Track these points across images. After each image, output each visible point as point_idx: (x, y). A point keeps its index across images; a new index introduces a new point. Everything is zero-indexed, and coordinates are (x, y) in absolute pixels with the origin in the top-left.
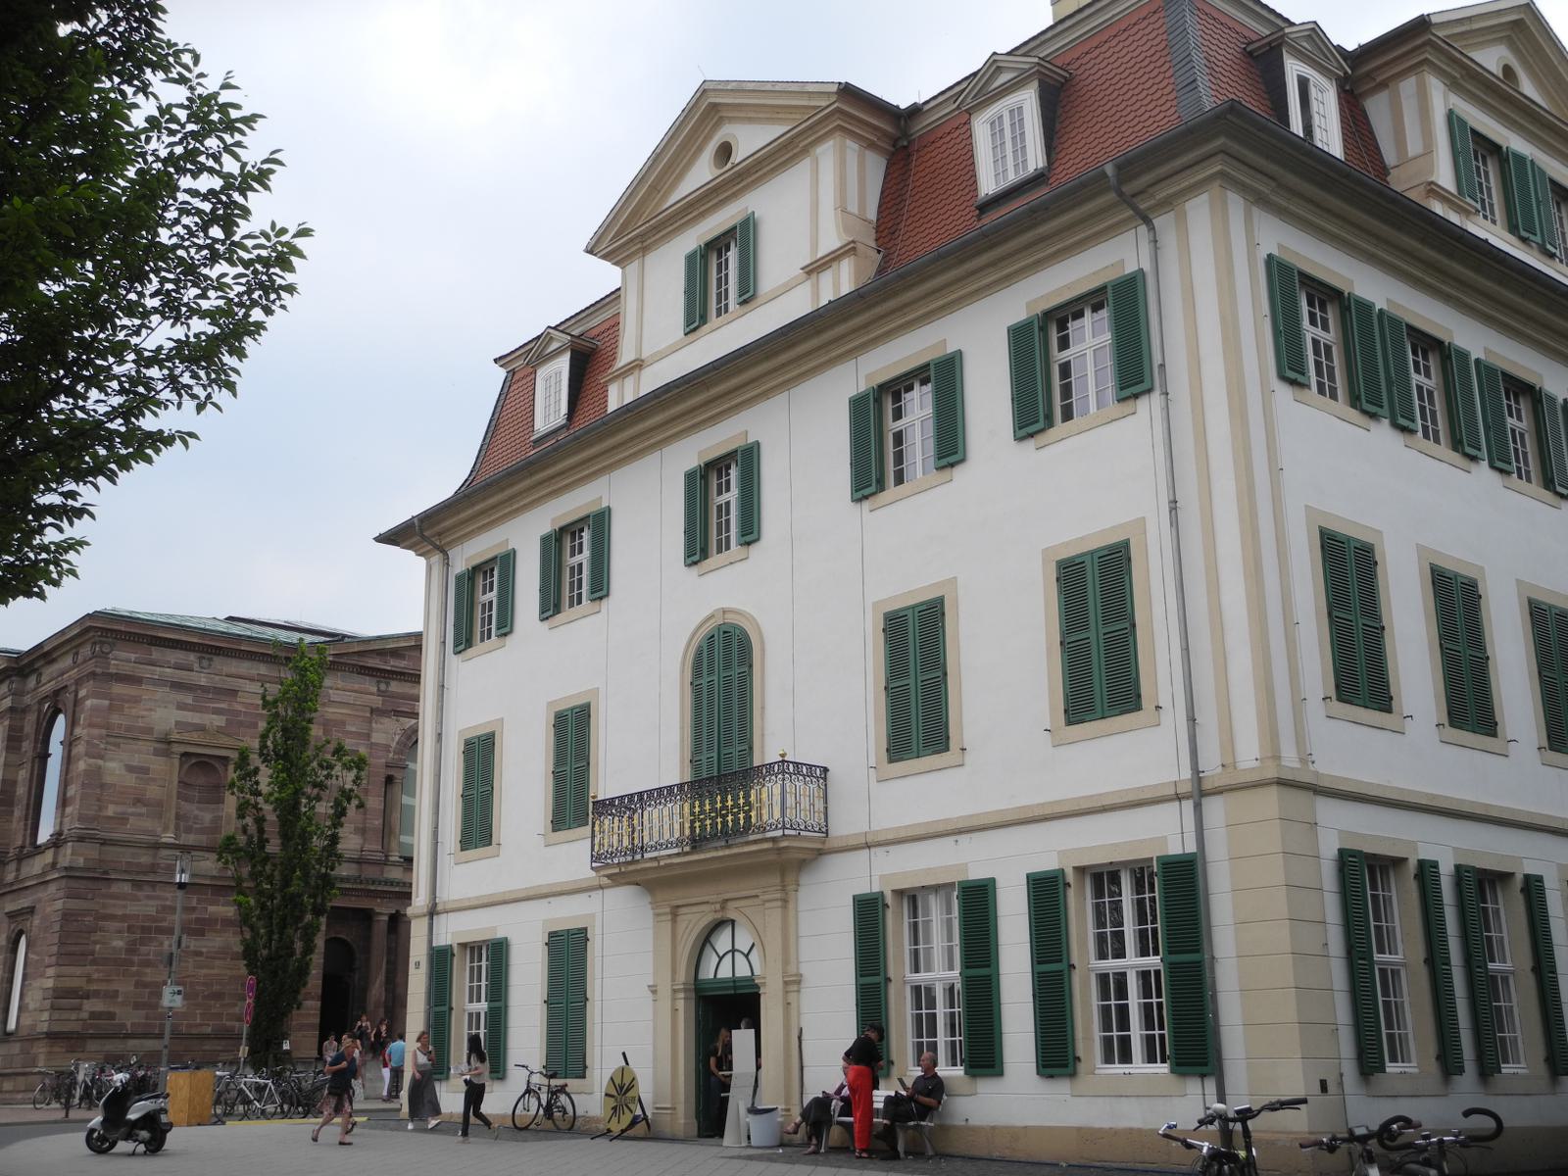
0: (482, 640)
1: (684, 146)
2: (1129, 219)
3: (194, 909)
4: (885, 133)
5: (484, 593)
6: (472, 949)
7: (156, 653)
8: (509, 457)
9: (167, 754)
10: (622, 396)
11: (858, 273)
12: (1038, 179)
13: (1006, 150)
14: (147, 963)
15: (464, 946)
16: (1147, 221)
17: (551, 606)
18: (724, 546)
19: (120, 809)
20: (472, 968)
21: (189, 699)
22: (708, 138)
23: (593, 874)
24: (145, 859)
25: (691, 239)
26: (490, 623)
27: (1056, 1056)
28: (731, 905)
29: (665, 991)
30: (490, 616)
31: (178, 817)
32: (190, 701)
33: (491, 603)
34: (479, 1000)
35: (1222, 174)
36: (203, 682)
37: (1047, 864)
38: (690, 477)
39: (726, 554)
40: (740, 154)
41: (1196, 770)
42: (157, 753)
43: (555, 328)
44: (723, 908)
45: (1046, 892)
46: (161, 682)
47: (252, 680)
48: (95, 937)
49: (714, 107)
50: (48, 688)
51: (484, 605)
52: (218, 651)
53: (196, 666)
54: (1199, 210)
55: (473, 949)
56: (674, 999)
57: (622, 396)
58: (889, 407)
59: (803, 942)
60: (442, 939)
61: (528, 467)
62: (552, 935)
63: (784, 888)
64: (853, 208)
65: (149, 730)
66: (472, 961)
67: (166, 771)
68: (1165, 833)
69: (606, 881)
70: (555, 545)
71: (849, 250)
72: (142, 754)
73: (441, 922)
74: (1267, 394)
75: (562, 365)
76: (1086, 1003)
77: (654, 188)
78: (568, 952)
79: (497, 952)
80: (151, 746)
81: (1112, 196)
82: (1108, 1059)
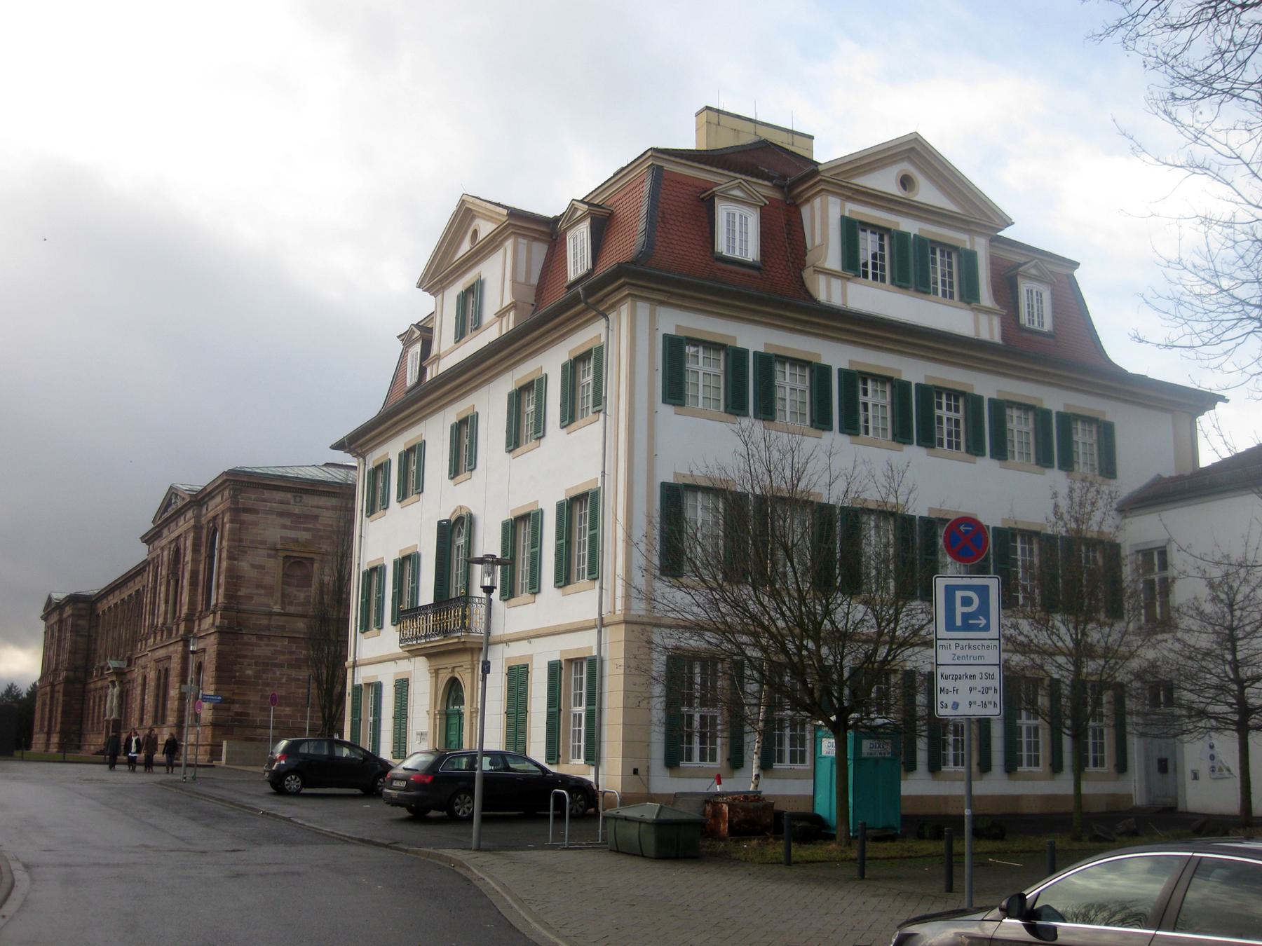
2: (595, 316)
3: (293, 653)
4: (543, 232)
7: (267, 494)
8: (399, 396)
9: (275, 557)
13: (578, 256)
14: (267, 685)
15: (570, 661)
17: (569, 416)
19: (249, 591)
21: (288, 522)
22: (466, 232)
24: (264, 622)
27: (1011, 766)
31: (283, 595)
32: (288, 523)
35: (629, 295)
36: (297, 511)
38: (510, 396)
40: (482, 236)
41: (600, 614)
42: (269, 556)
43: (582, 201)
44: (453, 671)
45: (555, 670)
46: (271, 512)
47: (327, 509)
48: (237, 667)
49: (468, 210)
50: (211, 514)
52: (306, 492)
53: (292, 501)
54: (625, 309)
60: (359, 681)
62: (510, 668)
64: (522, 278)
65: (264, 543)
67: (274, 566)
68: (585, 643)
71: (513, 306)
72: (260, 557)
74: (652, 412)
77: (446, 252)
78: (402, 687)
79: (377, 687)
80: (265, 552)
81: (582, 306)
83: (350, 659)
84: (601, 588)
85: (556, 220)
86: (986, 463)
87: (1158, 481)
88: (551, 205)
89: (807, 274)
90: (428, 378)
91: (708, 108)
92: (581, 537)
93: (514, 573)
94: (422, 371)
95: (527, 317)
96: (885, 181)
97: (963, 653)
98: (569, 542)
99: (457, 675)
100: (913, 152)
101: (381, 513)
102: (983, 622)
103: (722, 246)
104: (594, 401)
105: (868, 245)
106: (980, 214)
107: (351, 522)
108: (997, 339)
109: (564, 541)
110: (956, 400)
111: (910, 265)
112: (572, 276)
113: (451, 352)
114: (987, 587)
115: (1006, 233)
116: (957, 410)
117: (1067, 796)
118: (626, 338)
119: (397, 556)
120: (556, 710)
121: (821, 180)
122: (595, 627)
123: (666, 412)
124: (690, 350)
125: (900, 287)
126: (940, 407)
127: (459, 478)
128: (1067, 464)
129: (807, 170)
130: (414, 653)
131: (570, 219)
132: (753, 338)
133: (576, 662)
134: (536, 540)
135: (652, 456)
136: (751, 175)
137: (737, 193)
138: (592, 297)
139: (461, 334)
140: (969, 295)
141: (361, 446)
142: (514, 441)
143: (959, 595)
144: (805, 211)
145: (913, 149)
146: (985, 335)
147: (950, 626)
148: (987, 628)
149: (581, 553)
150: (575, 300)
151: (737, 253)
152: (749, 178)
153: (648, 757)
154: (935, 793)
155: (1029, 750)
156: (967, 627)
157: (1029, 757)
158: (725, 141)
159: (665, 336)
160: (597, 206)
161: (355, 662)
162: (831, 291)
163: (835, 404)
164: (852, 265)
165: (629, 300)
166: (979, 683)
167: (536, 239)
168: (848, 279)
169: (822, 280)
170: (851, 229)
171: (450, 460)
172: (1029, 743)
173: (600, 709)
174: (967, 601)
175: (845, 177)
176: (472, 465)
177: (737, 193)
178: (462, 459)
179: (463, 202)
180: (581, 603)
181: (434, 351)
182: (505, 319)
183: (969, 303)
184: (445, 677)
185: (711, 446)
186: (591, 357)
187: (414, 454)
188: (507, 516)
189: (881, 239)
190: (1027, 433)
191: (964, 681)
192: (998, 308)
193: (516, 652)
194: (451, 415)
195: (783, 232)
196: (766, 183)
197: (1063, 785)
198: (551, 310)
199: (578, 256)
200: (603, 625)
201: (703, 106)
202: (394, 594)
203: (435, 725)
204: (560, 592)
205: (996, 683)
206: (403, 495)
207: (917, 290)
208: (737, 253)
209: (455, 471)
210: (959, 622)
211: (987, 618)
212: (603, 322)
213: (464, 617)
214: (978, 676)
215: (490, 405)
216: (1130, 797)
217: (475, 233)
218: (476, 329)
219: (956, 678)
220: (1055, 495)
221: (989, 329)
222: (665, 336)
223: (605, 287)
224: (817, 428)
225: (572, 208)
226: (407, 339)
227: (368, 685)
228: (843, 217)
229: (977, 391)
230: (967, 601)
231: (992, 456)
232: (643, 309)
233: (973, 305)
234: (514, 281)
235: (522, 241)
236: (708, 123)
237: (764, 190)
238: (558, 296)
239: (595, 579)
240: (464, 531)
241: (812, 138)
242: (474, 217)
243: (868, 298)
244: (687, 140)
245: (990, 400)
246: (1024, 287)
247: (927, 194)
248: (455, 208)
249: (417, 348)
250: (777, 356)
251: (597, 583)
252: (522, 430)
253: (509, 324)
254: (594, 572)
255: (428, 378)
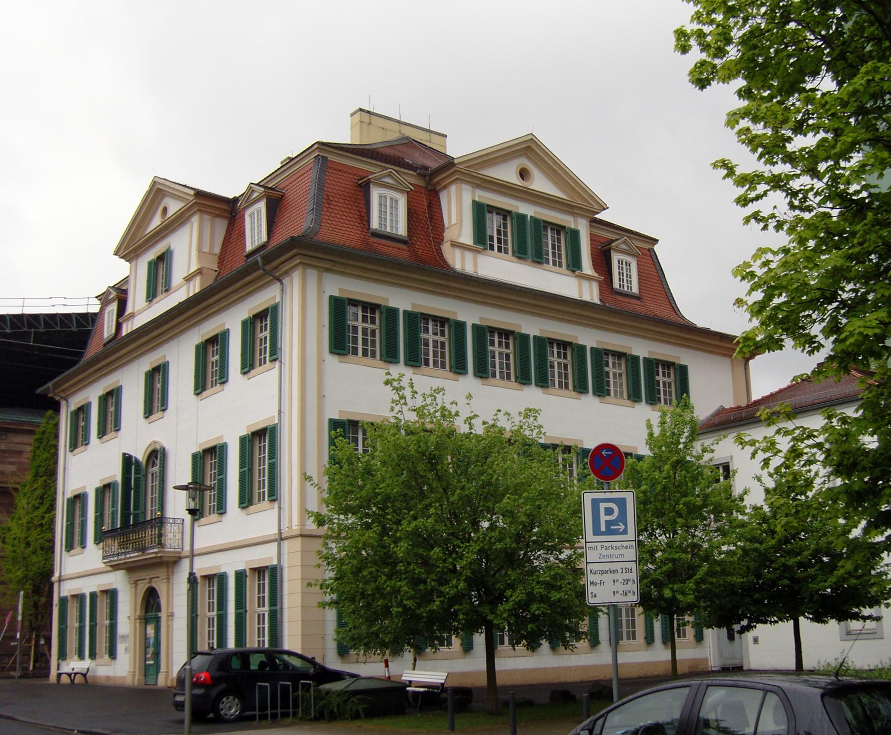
0: (260, 365)
1: (147, 213)
4: (225, 210)
5: (261, 332)
6: (259, 572)
10: (127, 330)
11: (202, 283)
12: (263, 247)
16: (280, 280)
17: (248, 366)
18: (262, 362)
20: (259, 585)
22: (157, 208)
23: (104, 565)
25: (151, 255)
26: (265, 353)
28: (153, 580)
29: (132, 618)
30: (265, 347)
33: (266, 338)
34: (264, 606)
35: (300, 263)
37: (241, 567)
38: (197, 347)
39: (263, 366)
40: (170, 213)
41: (280, 530)
43: (258, 185)
44: (150, 582)
49: (159, 190)
51: (261, 340)
54: (296, 276)
55: (209, 578)
56: (135, 623)
57: (127, 330)
58: (258, 325)
59: (175, 598)
60: (65, 593)
61: (243, 273)
63: (168, 572)
64: (206, 249)
66: (259, 580)
68: (266, 555)
69: (109, 568)
70: (250, 326)
71: (199, 272)
73: (197, 560)
74: (321, 361)
75: (262, 205)
76: (252, 627)
77: (139, 227)
81: (261, 272)
82: (628, 639)
83: (57, 574)
84: (280, 508)
85: (236, 200)
86: (590, 400)
87: (722, 411)
88: (231, 190)
89: (446, 248)
90: (124, 333)
91: (361, 110)
92: (261, 468)
93: (205, 495)
94: (119, 326)
95: (210, 281)
96: (508, 174)
97: (610, 552)
98: (251, 470)
99: (154, 585)
100: (529, 149)
101: (83, 448)
102: (622, 527)
103: (375, 224)
104: (271, 352)
105: (493, 223)
106: (586, 205)
107: (56, 455)
108: (596, 300)
109: (246, 469)
110: (565, 349)
111: (530, 242)
112: (249, 248)
113: (143, 312)
114: (624, 499)
115: (601, 216)
116: (373, 322)
117: (608, 665)
118: (300, 303)
119: (98, 484)
120: (242, 611)
121: (456, 171)
122: (275, 540)
123: (332, 361)
124: (351, 310)
125: (520, 258)
126: (492, 344)
127: (152, 417)
128: (653, 399)
129: (442, 162)
130: (116, 567)
131: (248, 198)
132: (403, 300)
133: (259, 571)
134: (222, 469)
135: (321, 397)
136: (399, 166)
137: (388, 180)
138: (268, 264)
139: (152, 295)
140: (575, 265)
141: (64, 391)
142: (201, 386)
143: (603, 506)
144: (443, 197)
145: (529, 147)
146: (586, 298)
147: (597, 532)
148: (625, 532)
149: (261, 477)
150: (254, 267)
151: (626, 289)
152: (397, 168)
153: (324, 648)
154: (555, 665)
155: (628, 627)
156: (609, 532)
157: (628, 632)
158: (374, 138)
159: (331, 297)
160: (271, 188)
161: (60, 576)
162: (461, 262)
163: (471, 352)
164: (482, 240)
165: (300, 268)
166: (620, 577)
167: (218, 216)
168: (479, 252)
169: (458, 252)
170: (480, 211)
171: (145, 402)
172: (627, 621)
173: (282, 609)
174: (609, 511)
175: (472, 171)
176: (164, 407)
177: (388, 180)
178: (155, 400)
179: (154, 183)
180: (262, 521)
181: (129, 310)
182: (192, 283)
183: (574, 272)
184: (143, 587)
185: (368, 390)
186: (268, 316)
187: (112, 397)
188: (197, 449)
189: (505, 219)
190: (620, 375)
191: (609, 574)
192: (597, 275)
193: (203, 566)
194: (146, 363)
195: (426, 215)
196: (411, 172)
197: (660, 654)
198: (235, 274)
199: (255, 231)
200: (282, 539)
201: (357, 108)
202: (96, 517)
203: (135, 628)
204: (244, 512)
205: (633, 576)
206: (102, 433)
207: (535, 262)
208: (626, 289)
209: (149, 412)
210: (603, 529)
211: (625, 524)
212: (277, 286)
213: (160, 535)
214: (620, 571)
215: (181, 358)
216: (706, 660)
217: (165, 210)
218: (167, 291)
219: (603, 572)
220: (649, 426)
221: (590, 293)
222: (331, 297)
223: (280, 256)
224: (386, 361)
225: (250, 190)
226: (104, 299)
227: (74, 596)
228: (474, 201)
229: (581, 342)
230: (609, 511)
231: (594, 394)
232: (312, 274)
233: (577, 273)
234: (200, 251)
235: (207, 217)
236: (362, 122)
237: (410, 179)
238: (239, 263)
239: (274, 500)
240: (158, 462)
241: (446, 136)
242: (164, 196)
243: (499, 267)
244: (344, 136)
245: (592, 348)
246: (615, 258)
247: (540, 183)
248: (148, 189)
249: (114, 307)
250: (350, 300)
251: (276, 505)
252: (209, 373)
253: (196, 287)
254: (274, 495)
255: (124, 333)
